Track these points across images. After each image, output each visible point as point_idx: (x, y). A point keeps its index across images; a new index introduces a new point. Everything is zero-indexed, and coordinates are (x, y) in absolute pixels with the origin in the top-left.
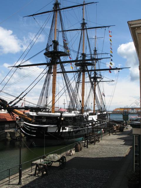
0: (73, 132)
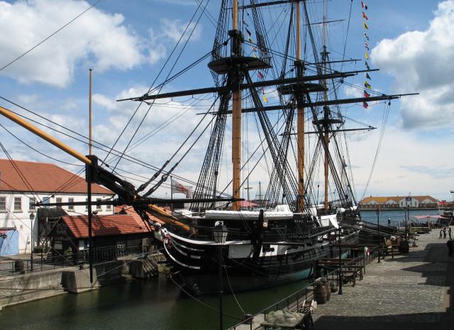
0: (289, 257)
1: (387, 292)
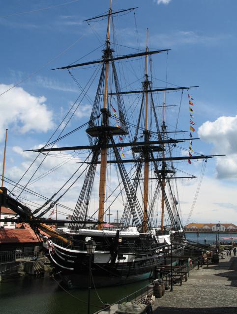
0: (136, 264)
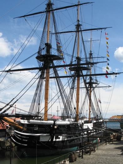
0: (67, 141)
1: (102, 158)
